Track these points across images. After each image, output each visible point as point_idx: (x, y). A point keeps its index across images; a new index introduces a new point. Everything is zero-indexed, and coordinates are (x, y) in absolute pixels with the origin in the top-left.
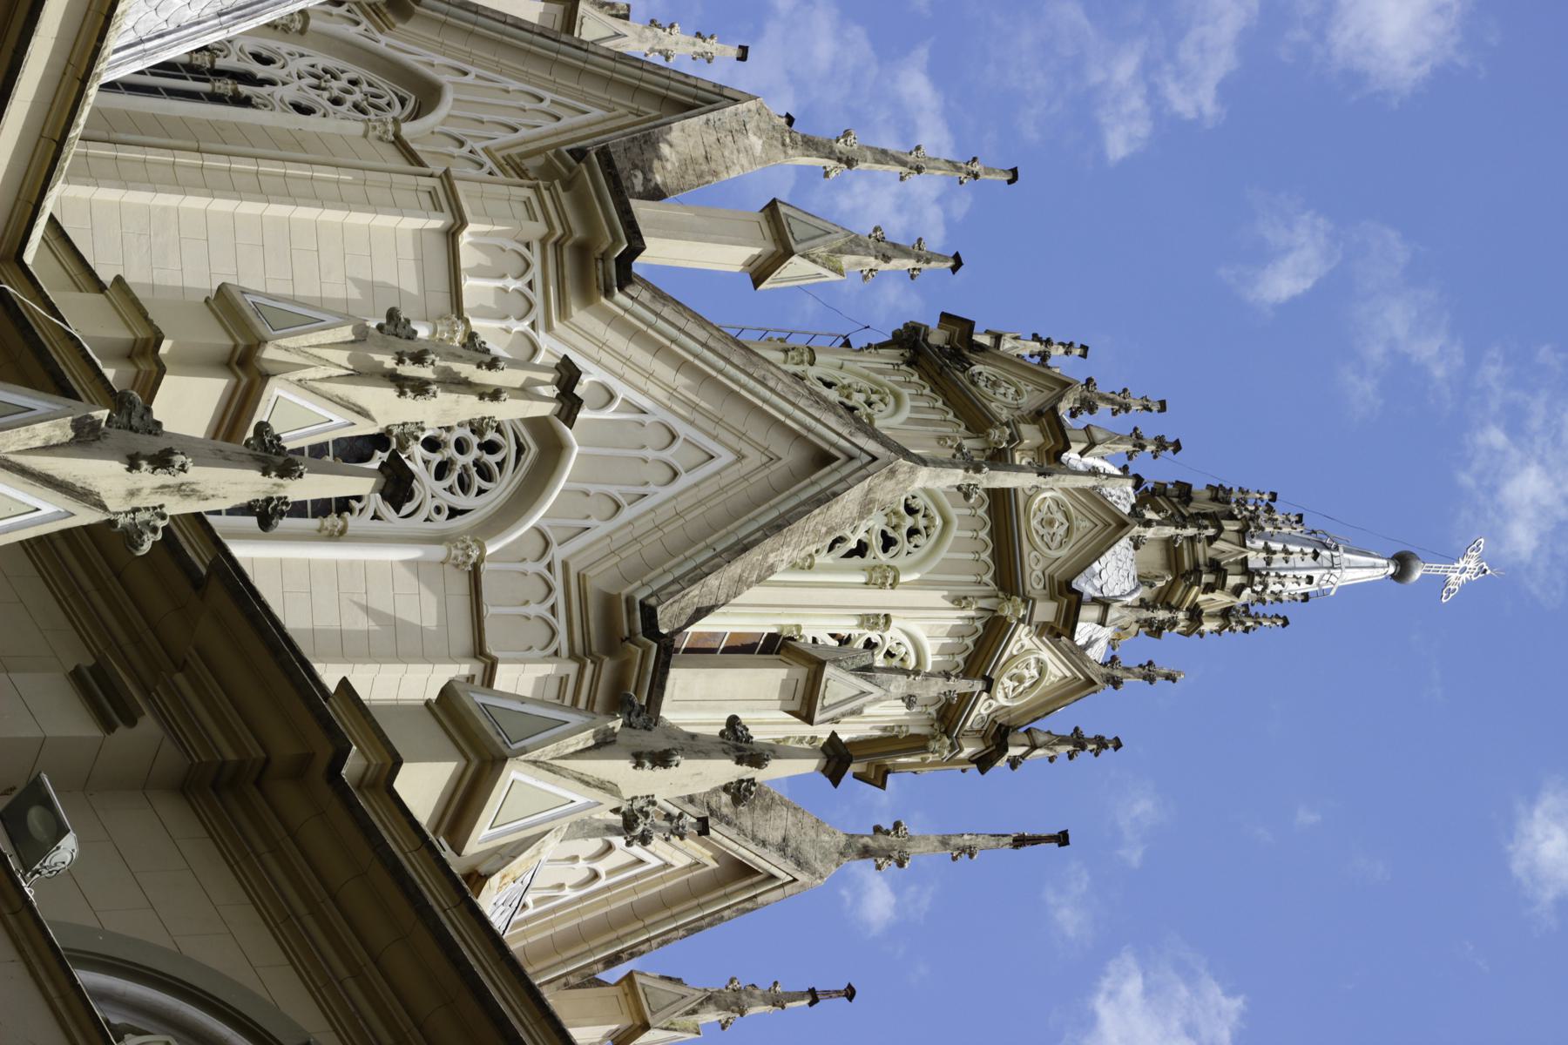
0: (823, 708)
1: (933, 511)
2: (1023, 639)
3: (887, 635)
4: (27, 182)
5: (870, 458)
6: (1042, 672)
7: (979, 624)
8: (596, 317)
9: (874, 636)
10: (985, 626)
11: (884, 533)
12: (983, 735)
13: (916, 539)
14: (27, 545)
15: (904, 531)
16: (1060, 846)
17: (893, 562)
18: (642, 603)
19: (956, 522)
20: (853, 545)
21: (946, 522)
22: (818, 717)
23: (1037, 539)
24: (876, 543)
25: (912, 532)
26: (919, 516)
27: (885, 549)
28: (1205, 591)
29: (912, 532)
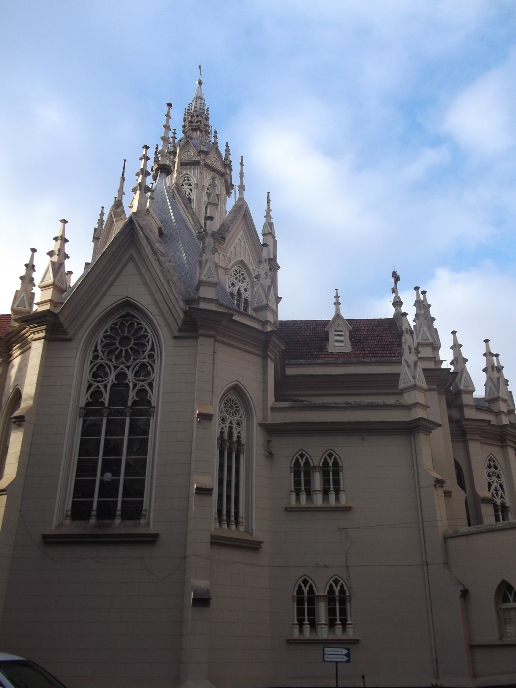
0: (216, 202)
1: (185, 176)
2: (208, 161)
3: (206, 186)
4: (251, 349)
5: (131, 261)
6: (214, 157)
7: (205, 169)
8: (3, 473)
9: (206, 188)
10: (205, 168)
11: (188, 186)
12: (225, 168)
13: (189, 180)
14: (25, 340)
15: (188, 182)
16: (232, 170)
17: (193, 184)
18: (197, 234)
19: (187, 172)
20: (190, 192)
21: (187, 174)
22: (217, 203)
23: (190, 157)
24: (190, 187)
25: (188, 180)
26: (185, 179)
27: (191, 185)
28: (202, 124)
29: (188, 180)
